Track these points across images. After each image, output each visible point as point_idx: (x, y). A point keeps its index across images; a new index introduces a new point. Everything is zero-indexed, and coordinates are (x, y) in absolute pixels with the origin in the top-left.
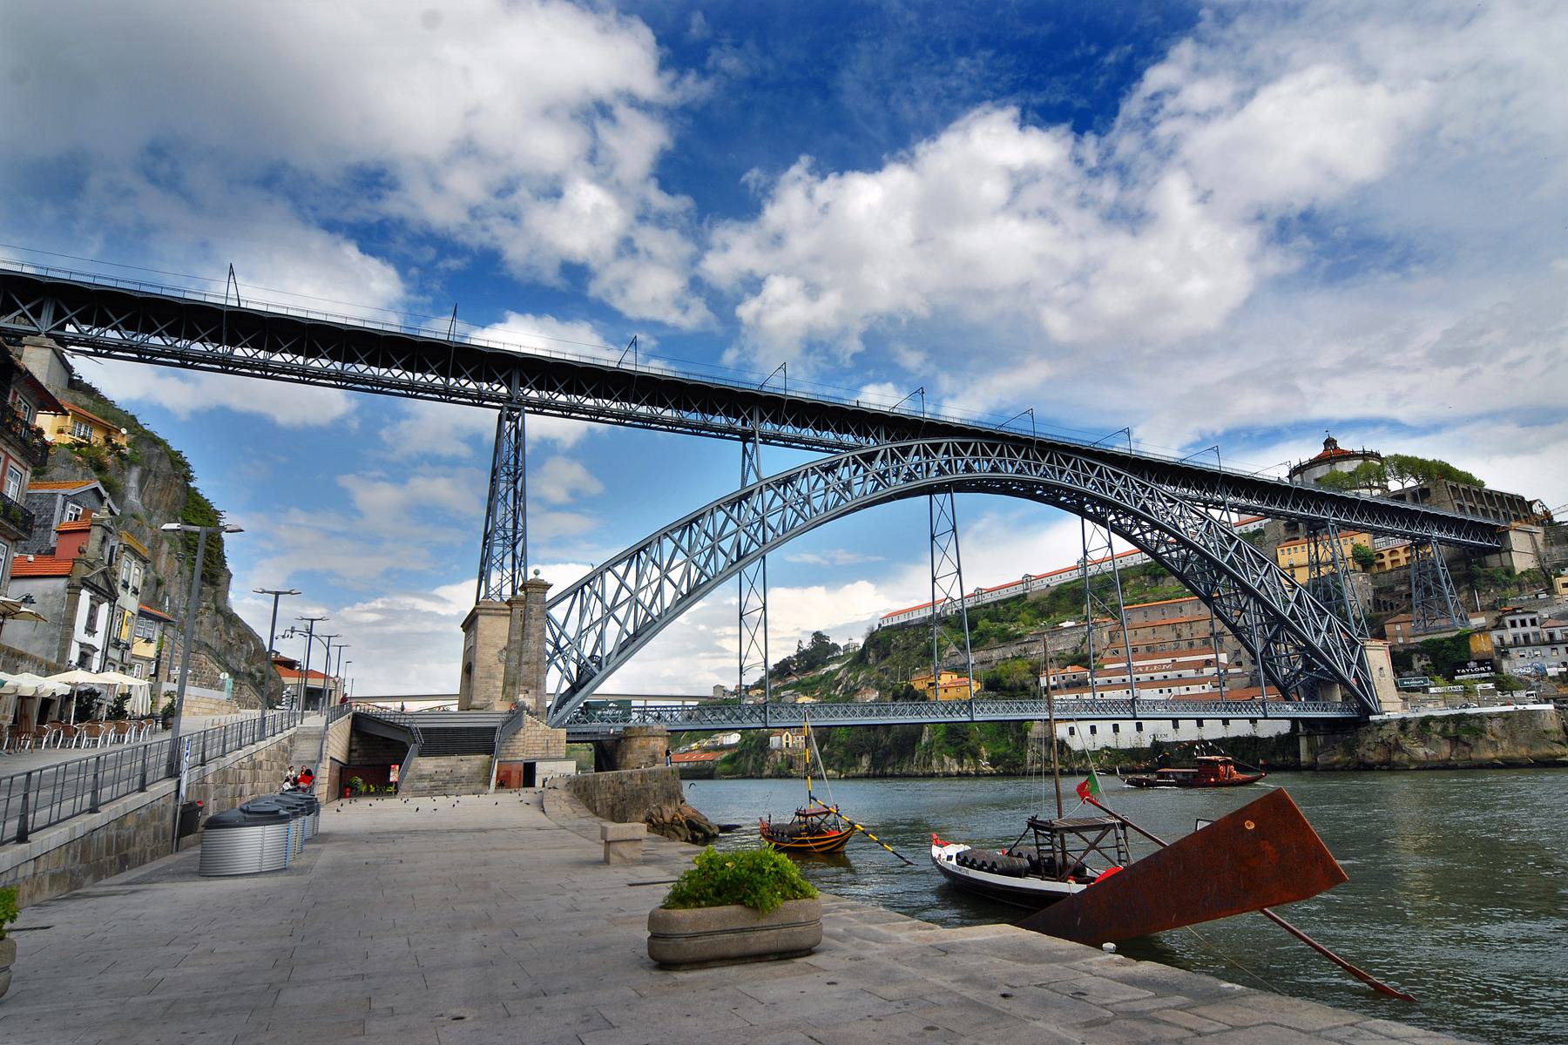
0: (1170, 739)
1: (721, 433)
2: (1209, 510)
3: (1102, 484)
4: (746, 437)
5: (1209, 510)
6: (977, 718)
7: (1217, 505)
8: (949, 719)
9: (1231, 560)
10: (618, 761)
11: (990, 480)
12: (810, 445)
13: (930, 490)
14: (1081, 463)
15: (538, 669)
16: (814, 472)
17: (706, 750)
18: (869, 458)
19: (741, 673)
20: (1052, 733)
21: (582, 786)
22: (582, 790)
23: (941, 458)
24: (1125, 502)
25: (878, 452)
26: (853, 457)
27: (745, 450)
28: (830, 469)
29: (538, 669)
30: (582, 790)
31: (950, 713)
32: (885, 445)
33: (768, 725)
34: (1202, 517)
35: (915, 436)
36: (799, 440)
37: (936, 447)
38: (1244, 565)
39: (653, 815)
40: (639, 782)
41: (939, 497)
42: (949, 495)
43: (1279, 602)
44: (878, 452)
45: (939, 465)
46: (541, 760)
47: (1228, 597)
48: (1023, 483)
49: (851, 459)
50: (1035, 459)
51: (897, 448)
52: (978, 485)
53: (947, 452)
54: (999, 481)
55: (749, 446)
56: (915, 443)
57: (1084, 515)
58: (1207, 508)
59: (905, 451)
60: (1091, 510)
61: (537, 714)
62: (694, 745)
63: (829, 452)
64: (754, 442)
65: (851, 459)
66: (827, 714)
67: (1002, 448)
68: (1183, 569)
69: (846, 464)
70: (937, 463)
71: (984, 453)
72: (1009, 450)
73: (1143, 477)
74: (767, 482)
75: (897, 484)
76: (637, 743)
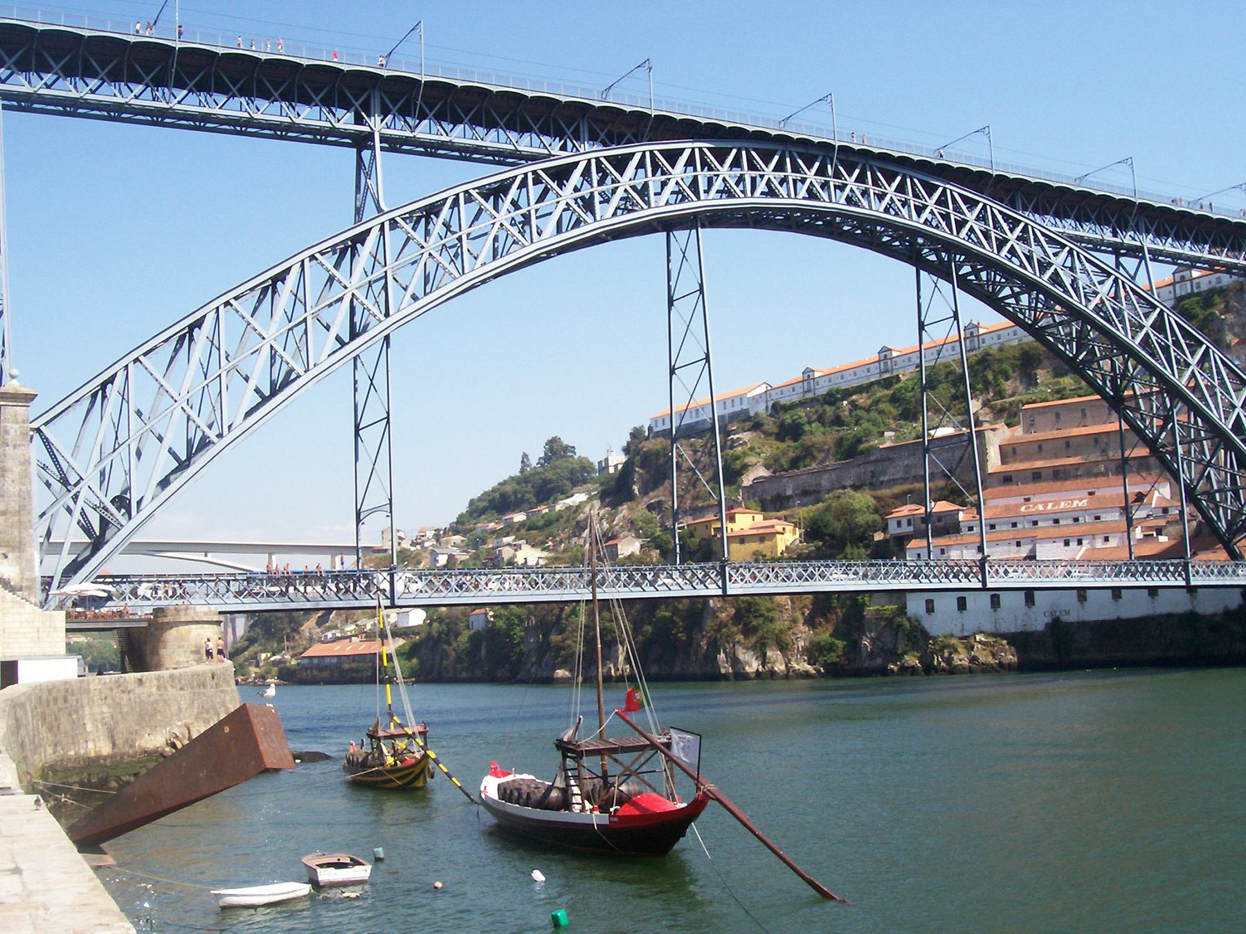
0: (1072, 618)
1: (320, 136)
2: (1122, 260)
3: (946, 217)
4: (361, 142)
5: (1122, 260)
6: (733, 589)
7: (1135, 252)
8: (636, 593)
9: (1146, 342)
10: (149, 659)
11: (806, 212)
12: (467, 154)
13: (667, 225)
14: (913, 184)
15: (20, 522)
16: (469, 199)
17: (369, 636)
18: (561, 174)
19: (358, 520)
20: (902, 610)
21: (61, 695)
22: (60, 701)
23: (679, 172)
24: (981, 244)
25: (576, 164)
26: (534, 172)
27: (360, 160)
28: (496, 192)
29: (20, 522)
30: (60, 701)
31: (956, 576)
32: (589, 152)
33: (397, 602)
34: (1103, 271)
35: (638, 138)
36: (450, 146)
37: (672, 157)
38: (1165, 350)
39: (177, 737)
40: (154, 690)
41: (680, 235)
42: (694, 231)
43: (1217, 408)
44: (576, 164)
45: (769, 183)
46: (29, 657)
47: (1146, 396)
48: (862, 221)
49: (530, 177)
50: (837, 175)
51: (605, 157)
52: (787, 218)
53: (691, 162)
54: (821, 214)
55: (366, 154)
56: (638, 150)
57: (920, 263)
58: (1118, 255)
59: (620, 163)
60: (933, 258)
61: (20, 590)
62: (350, 628)
63: (499, 163)
64: (373, 148)
65: (530, 177)
66: (754, 577)
67: (738, 156)
68: (1078, 352)
69: (524, 184)
70: (721, 178)
71: (752, 167)
72: (750, 158)
73: (1013, 206)
74: (391, 215)
75: (605, 217)
76: (171, 635)
